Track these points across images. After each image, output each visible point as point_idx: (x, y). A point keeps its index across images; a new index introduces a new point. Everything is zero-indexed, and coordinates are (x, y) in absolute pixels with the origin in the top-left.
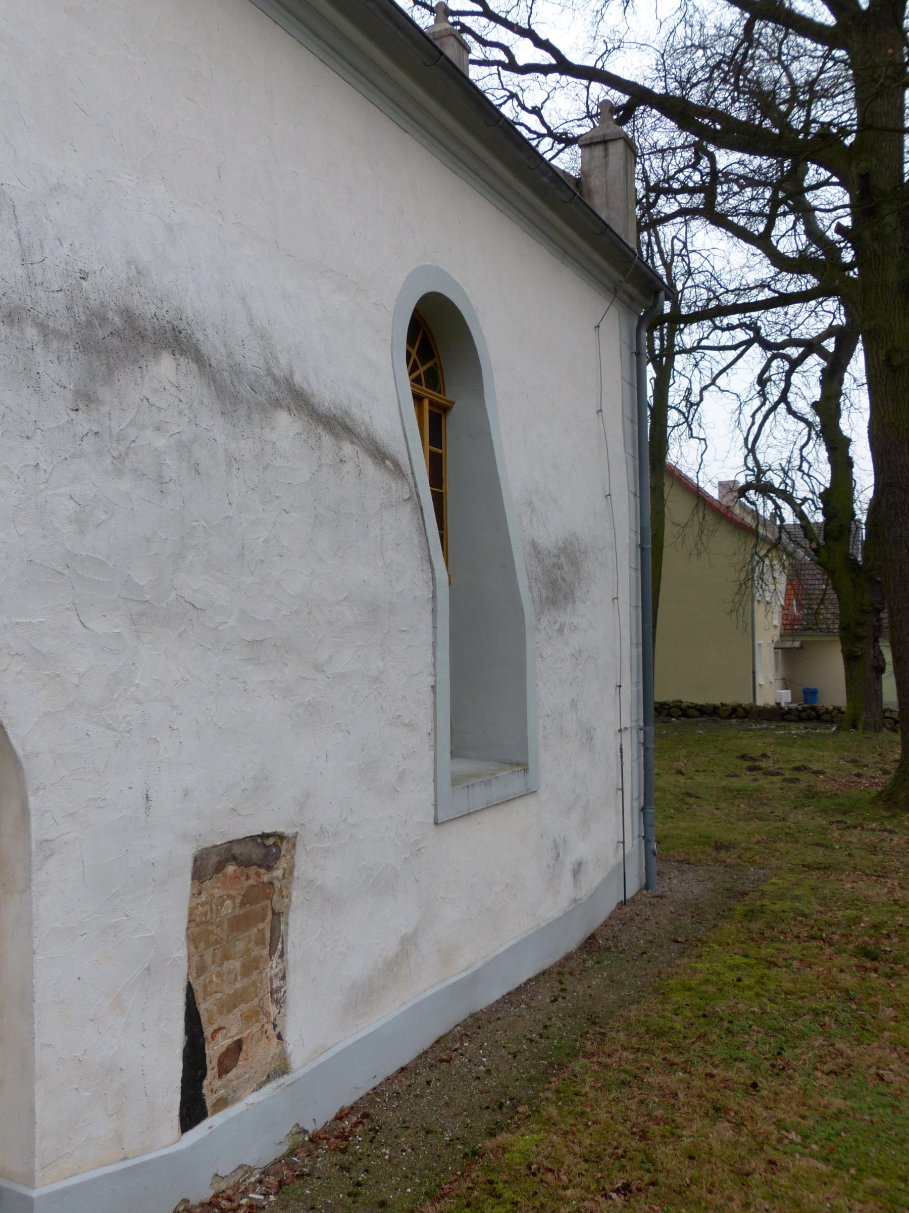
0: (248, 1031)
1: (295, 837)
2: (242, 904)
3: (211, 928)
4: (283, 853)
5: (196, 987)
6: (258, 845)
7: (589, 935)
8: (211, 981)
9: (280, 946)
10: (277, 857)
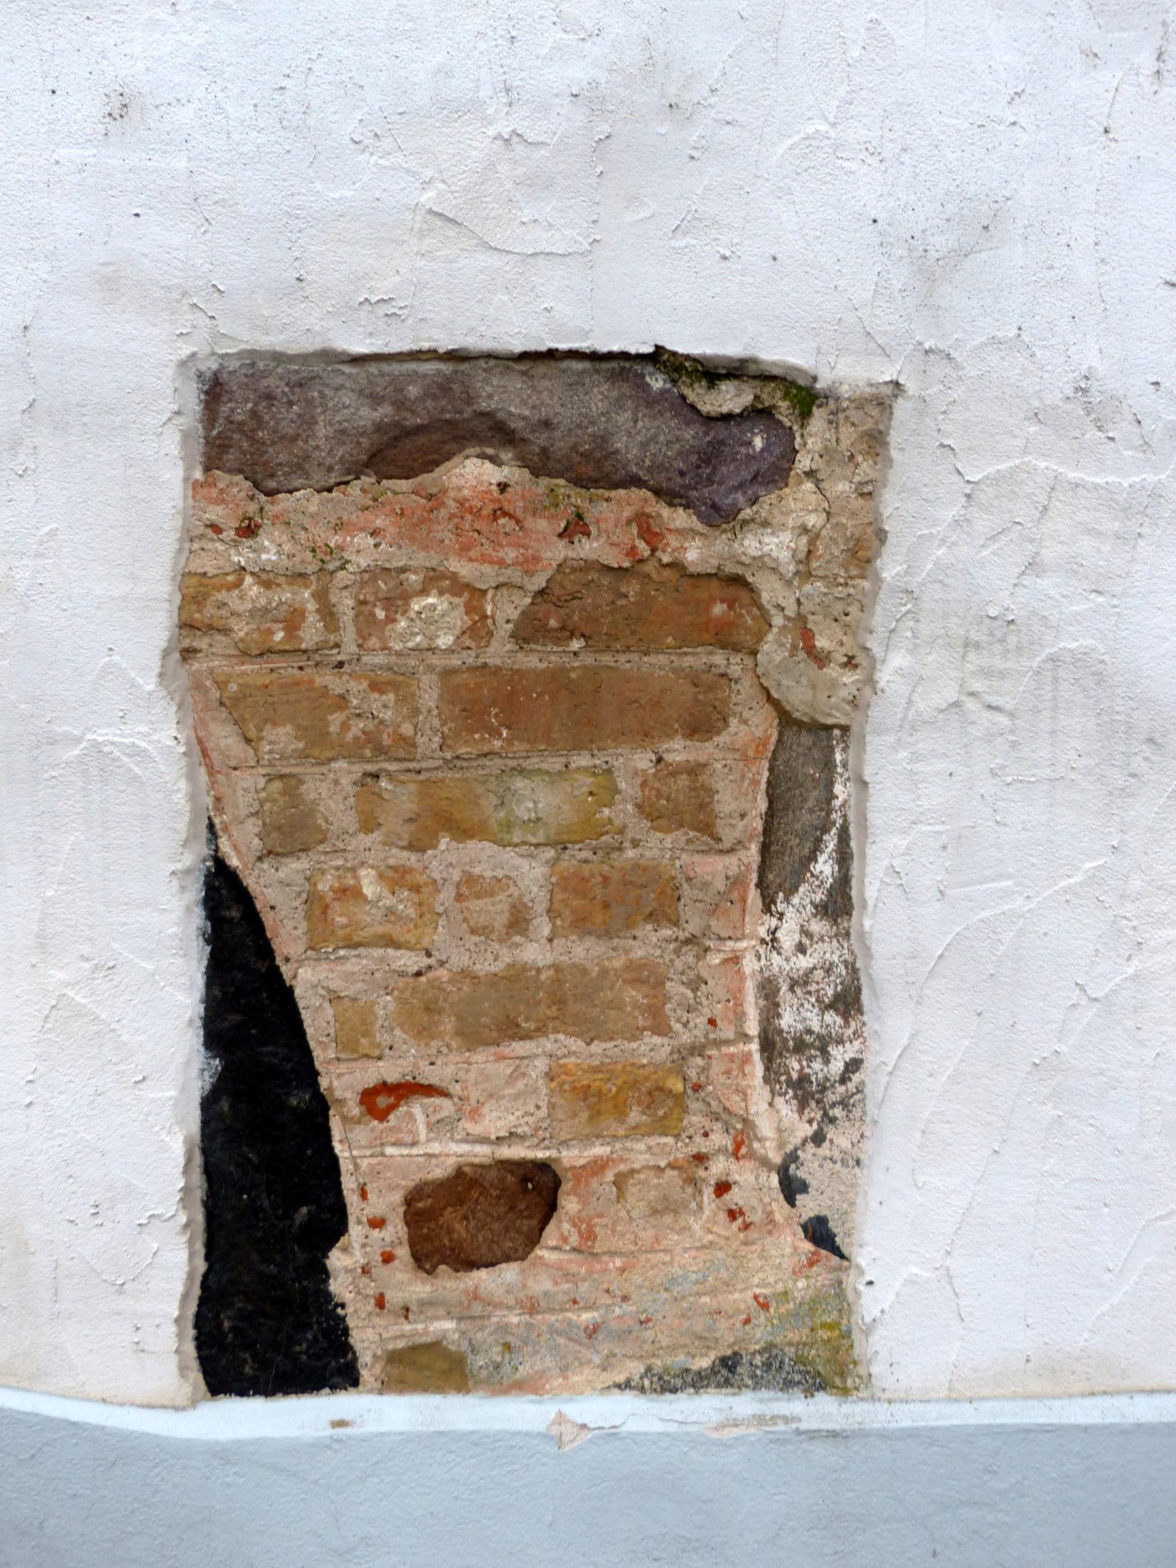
0: (600, 1150)
1: (884, 399)
2: (528, 632)
3: (328, 679)
4: (804, 462)
5: (273, 888)
6: (651, 401)
7: (668, 1396)
8: (349, 893)
9: (825, 866)
10: (776, 472)
